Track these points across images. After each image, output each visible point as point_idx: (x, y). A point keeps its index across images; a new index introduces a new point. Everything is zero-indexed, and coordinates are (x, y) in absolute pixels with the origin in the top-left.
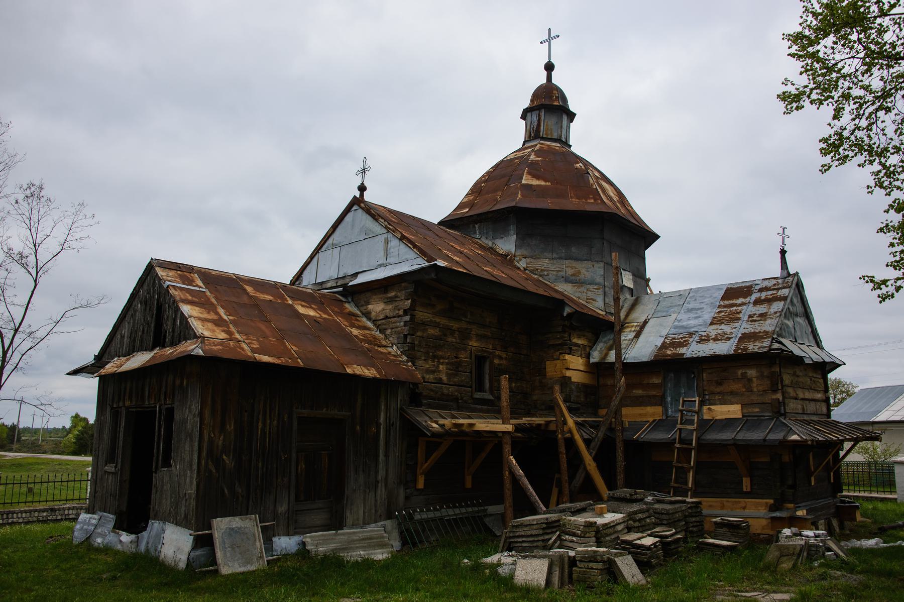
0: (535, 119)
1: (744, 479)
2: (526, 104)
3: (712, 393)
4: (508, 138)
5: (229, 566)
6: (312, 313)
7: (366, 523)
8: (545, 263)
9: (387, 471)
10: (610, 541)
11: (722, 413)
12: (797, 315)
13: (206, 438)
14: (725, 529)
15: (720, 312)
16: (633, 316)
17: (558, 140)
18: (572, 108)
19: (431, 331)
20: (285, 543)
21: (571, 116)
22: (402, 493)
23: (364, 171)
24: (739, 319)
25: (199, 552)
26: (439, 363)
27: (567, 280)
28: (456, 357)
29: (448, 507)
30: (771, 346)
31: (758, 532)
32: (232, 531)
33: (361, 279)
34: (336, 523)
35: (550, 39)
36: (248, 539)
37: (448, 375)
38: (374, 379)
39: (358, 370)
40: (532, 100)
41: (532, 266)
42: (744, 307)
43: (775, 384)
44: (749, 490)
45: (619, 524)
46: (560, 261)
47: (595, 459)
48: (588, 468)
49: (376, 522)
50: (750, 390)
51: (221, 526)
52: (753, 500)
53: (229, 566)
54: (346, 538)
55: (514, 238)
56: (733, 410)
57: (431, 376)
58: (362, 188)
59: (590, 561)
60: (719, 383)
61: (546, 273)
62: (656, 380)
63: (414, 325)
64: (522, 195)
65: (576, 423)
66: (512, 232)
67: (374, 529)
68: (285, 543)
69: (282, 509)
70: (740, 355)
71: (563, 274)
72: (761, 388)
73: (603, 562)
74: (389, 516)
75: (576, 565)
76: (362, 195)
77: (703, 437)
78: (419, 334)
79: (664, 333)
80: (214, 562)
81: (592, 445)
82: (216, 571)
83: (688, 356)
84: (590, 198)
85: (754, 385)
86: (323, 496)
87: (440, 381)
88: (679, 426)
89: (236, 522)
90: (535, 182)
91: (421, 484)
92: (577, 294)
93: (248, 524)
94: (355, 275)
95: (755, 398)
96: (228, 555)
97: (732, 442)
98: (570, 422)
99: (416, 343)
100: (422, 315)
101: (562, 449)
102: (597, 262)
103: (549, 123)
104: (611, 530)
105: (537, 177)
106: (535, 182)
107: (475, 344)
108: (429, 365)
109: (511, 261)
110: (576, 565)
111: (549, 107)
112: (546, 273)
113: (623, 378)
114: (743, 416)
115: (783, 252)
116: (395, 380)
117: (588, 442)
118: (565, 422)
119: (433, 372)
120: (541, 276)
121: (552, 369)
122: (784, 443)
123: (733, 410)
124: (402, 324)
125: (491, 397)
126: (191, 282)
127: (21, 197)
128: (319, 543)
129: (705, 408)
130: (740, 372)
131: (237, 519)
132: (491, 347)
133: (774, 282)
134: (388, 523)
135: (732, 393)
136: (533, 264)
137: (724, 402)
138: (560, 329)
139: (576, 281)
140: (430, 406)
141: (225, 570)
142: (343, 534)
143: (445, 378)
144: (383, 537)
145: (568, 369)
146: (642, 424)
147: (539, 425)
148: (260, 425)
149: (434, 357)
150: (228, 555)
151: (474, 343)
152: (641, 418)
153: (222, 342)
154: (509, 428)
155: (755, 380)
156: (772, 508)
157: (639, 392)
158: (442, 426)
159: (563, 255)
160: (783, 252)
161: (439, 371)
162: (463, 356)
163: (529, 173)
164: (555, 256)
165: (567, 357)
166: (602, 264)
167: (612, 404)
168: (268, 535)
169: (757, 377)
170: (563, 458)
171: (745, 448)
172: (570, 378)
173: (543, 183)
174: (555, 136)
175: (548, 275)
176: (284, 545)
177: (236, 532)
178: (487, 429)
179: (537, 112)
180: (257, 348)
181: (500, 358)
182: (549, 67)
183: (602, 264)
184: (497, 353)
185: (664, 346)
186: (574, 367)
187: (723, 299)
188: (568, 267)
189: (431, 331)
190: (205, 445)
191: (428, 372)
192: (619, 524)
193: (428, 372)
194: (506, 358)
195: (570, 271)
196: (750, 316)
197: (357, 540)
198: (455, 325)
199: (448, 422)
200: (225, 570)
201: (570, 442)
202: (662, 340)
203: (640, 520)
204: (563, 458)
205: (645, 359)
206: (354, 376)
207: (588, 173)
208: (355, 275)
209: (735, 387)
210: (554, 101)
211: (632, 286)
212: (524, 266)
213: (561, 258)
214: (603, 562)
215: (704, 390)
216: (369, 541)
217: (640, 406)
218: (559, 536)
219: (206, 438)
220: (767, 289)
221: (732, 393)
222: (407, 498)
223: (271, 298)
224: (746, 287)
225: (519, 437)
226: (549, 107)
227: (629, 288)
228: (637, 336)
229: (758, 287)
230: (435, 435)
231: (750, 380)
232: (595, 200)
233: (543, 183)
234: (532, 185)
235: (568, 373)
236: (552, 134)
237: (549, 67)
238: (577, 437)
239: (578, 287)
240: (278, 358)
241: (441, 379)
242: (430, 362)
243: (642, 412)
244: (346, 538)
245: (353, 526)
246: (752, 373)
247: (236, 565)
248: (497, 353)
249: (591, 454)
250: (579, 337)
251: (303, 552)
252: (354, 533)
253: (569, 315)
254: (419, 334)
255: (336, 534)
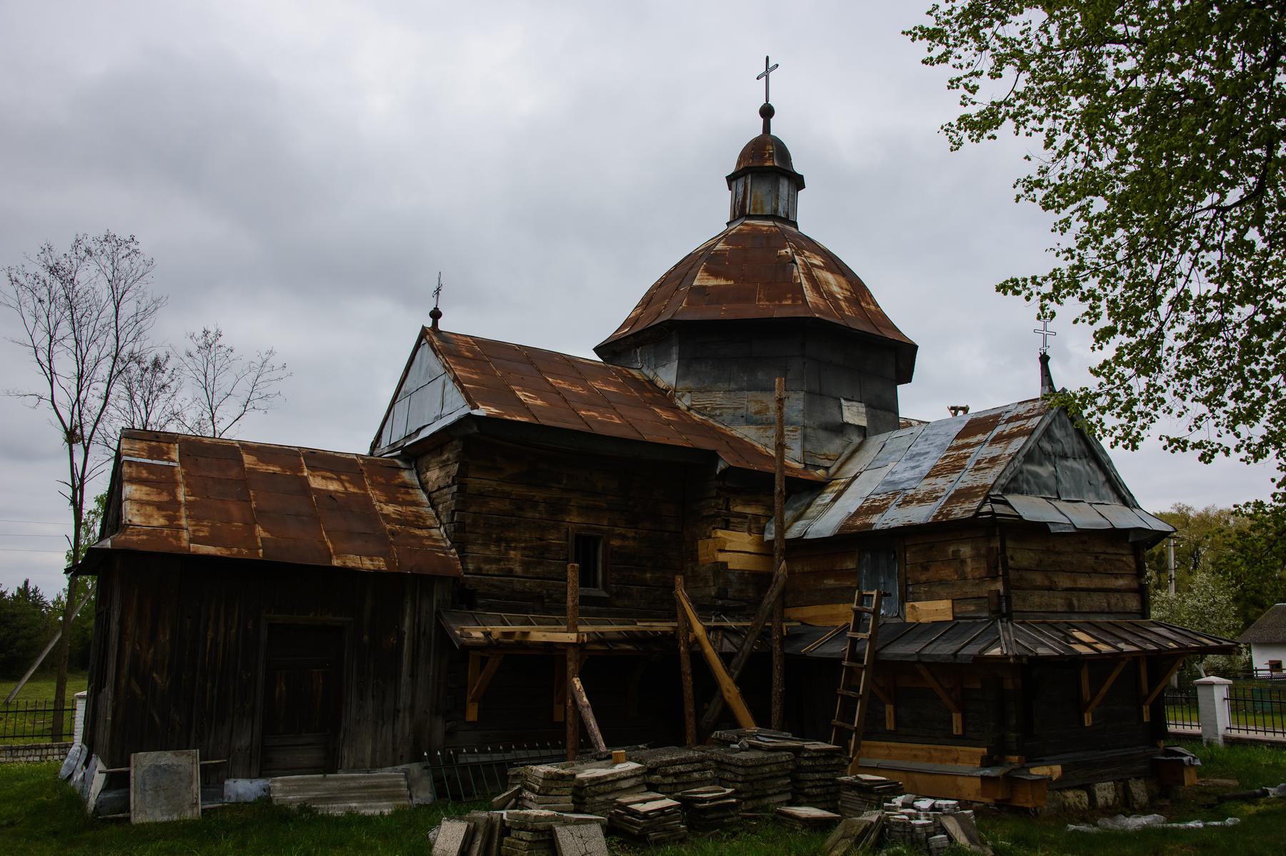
0: (741, 189)
1: (954, 715)
2: (731, 169)
3: (917, 583)
4: (708, 216)
5: (146, 811)
6: (333, 486)
7: (375, 766)
8: (718, 398)
9: (413, 697)
10: (604, 803)
11: (928, 613)
12: (1064, 456)
13: (128, 651)
14: (854, 793)
15: (945, 458)
16: (846, 468)
17: (774, 217)
18: (798, 167)
19: (494, 504)
20: (243, 788)
21: (798, 182)
22: (439, 728)
23: (438, 291)
24: (962, 467)
25: (110, 795)
26: (508, 548)
27: (748, 421)
28: (541, 539)
29: (518, 748)
30: (980, 508)
31: (972, 798)
32: (157, 770)
33: (425, 434)
34: (330, 765)
35: (766, 74)
36: (181, 780)
37: (523, 563)
38: (377, 574)
39: (353, 561)
40: (739, 163)
41: (698, 404)
42: (976, 449)
43: (996, 566)
44: (960, 732)
45: (625, 778)
46: (740, 394)
47: (738, 682)
48: (726, 695)
49: (394, 764)
50: (964, 578)
51: (143, 762)
52: (968, 749)
53: (146, 811)
54: (336, 784)
55: (675, 365)
56: (935, 609)
57: (494, 566)
58: (436, 315)
59: (521, 829)
60: (925, 568)
61: (718, 412)
62: (850, 565)
63: (464, 496)
64: (688, 303)
65: (708, 630)
66: (675, 356)
67: (389, 775)
68: (243, 788)
69: (243, 741)
70: (941, 523)
71: (742, 412)
72: (977, 574)
73: (535, 831)
74: (416, 757)
75: (509, 835)
76: (435, 324)
77: (885, 651)
78: (473, 509)
79: (866, 494)
80: (126, 807)
81: (735, 661)
82: (128, 819)
83: (878, 527)
84: (786, 299)
85: (969, 569)
86: (307, 726)
87: (510, 573)
88: (849, 634)
89: (167, 758)
90: (712, 282)
91: (472, 714)
92: (762, 441)
93: (187, 762)
94: (419, 431)
95: (969, 590)
96: (148, 799)
97: (915, 659)
98: (699, 628)
99: (469, 521)
100: (476, 482)
101: (686, 667)
102: (795, 391)
103: (760, 193)
104: (609, 788)
105: (716, 274)
106: (712, 282)
107: (576, 520)
108: (492, 551)
109: (672, 397)
110: (509, 835)
111: (765, 169)
112: (718, 412)
113: (784, 563)
114: (955, 618)
115: (1044, 359)
116: (412, 574)
117: (726, 658)
118: (690, 628)
119: (498, 561)
120: (711, 417)
121: (706, 552)
122: (980, 660)
123: (935, 609)
124: (449, 497)
125: (604, 594)
126: (160, 454)
127: (194, 350)
128: (287, 789)
129: (908, 605)
130: (951, 549)
131: (169, 754)
132: (606, 522)
133: (1030, 406)
134: (415, 768)
135: (942, 582)
136: (704, 400)
137: (931, 597)
138: (714, 493)
139: (751, 419)
140: (491, 608)
141: (137, 819)
142: (336, 779)
143: (518, 569)
144: (400, 786)
145: (721, 551)
146: (826, 629)
147: (665, 633)
148: (210, 634)
149: (498, 541)
150: (148, 799)
151: (574, 520)
152: (829, 625)
153: (153, 532)
154: (572, 637)
155: (969, 561)
156: (987, 762)
157: (830, 582)
158: (487, 634)
159: (745, 384)
160: (1044, 359)
161: (509, 560)
162: (553, 538)
163: (706, 270)
164: (733, 386)
165: (720, 533)
166: (802, 394)
167: (766, 601)
168: (212, 778)
169: (972, 558)
170: (688, 681)
171: (951, 668)
172: (725, 564)
173: (722, 282)
174: (768, 210)
175: (721, 415)
176: (241, 791)
177: (165, 770)
178: (544, 639)
179: (742, 179)
180: (205, 537)
181: (623, 537)
182: (767, 112)
183: (802, 394)
184: (618, 530)
185: (858, 513)
186: (736, 547)
187: (957, 437)
188: (751, 402)
189: (494, 504)
190: (127, 661)
191: (488, 560)
192: (625, 778)
193: (488, 560)
194: (634, 538)
195: (753, 408)
196: (978, 462)
197: (354, 788)
198: (538, 495)
199: (497, 630)
200: (137, 819)
201: (699, 658)
202: (859, 503)
203: (676, 775)
204: (688, 681)
205: (827, 534)
206: (344, 570)
207: (794, 262)
208: (419, 431)
209: (947, 573)
210: (766, 160)
211: (864, 423)
212: (688, 404)
213: (741, 389)
214: (535, 831)
215: (907, 579)
216: (367, 790)
217: (832, 603)
218: (520, 791)
219: (128, 651)
220: (1017, 418)
221: (942, 582)
222: (449, 733)
223: (277, 469)
224: (990, 417)
225: (628, 650)
226: (765, 169)
227: (859, 427)
228: (834, 500)
229: (1006, 417)
230: (477, 647)
231: (963, 562)
232: (794, 300)
233: (722, 282)
234: (705, 287)
235: (721, 557)
236: (762, 209)
237: (767, 112)
238: (709, 650)
239: (765, 430)
240: (229, 548)
241: (511, 570)
242: (493, 548)
243: (834, 612)
244: (336, 784)
245: (355, 769)
246: (966, 551)
247: (158, 812)
248: (618, 530)
249: (731, 675)
250: (747, 503)
251: (265, 800)
252: (353, 778)
253: (722, 471)
254: (473, 509)
255: (324, 779)
